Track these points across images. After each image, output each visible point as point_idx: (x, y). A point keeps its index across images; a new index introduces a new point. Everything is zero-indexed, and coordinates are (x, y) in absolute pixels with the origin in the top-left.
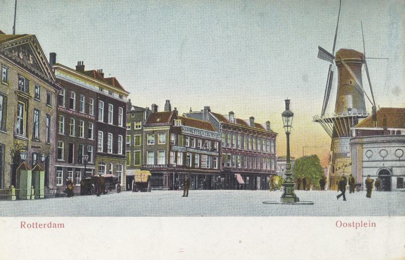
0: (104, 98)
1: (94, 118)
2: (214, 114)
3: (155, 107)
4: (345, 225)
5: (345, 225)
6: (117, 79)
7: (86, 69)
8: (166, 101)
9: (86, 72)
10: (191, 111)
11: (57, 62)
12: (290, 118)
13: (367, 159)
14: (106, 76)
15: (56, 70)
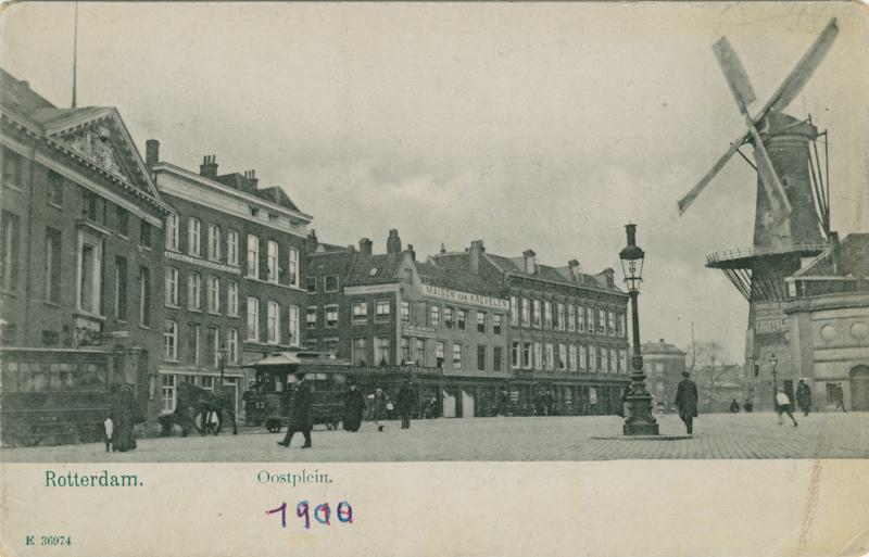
0: (257, 230)
1: (237, 271)
2: (492, 256)
3: (367, 244)
6: (283, 188)
7: (220, 172)
8: (391, 232)
9: (222, 177)
10: (443, 251)
11: (160, 160)
12: (638, 261)
13: (822, 344)
14: (261, 186)
15: (159, 176)
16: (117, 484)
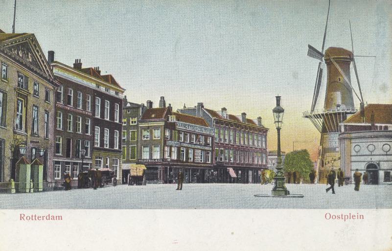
0: (101, 94)
1: (91, 114)
2: (207, 110)
3: (150, 103)
4: (334, 217)
5: (334, 217)
6: (113, 76)
7: (83, 67)
8: (161, 98)
9: (84, 69)
10: (185, 107)
11: (55, 60)
12: (281, 114)
13: (356, 154)
14: (102, 74)
15: (54, 68)
16: (59, 217)
